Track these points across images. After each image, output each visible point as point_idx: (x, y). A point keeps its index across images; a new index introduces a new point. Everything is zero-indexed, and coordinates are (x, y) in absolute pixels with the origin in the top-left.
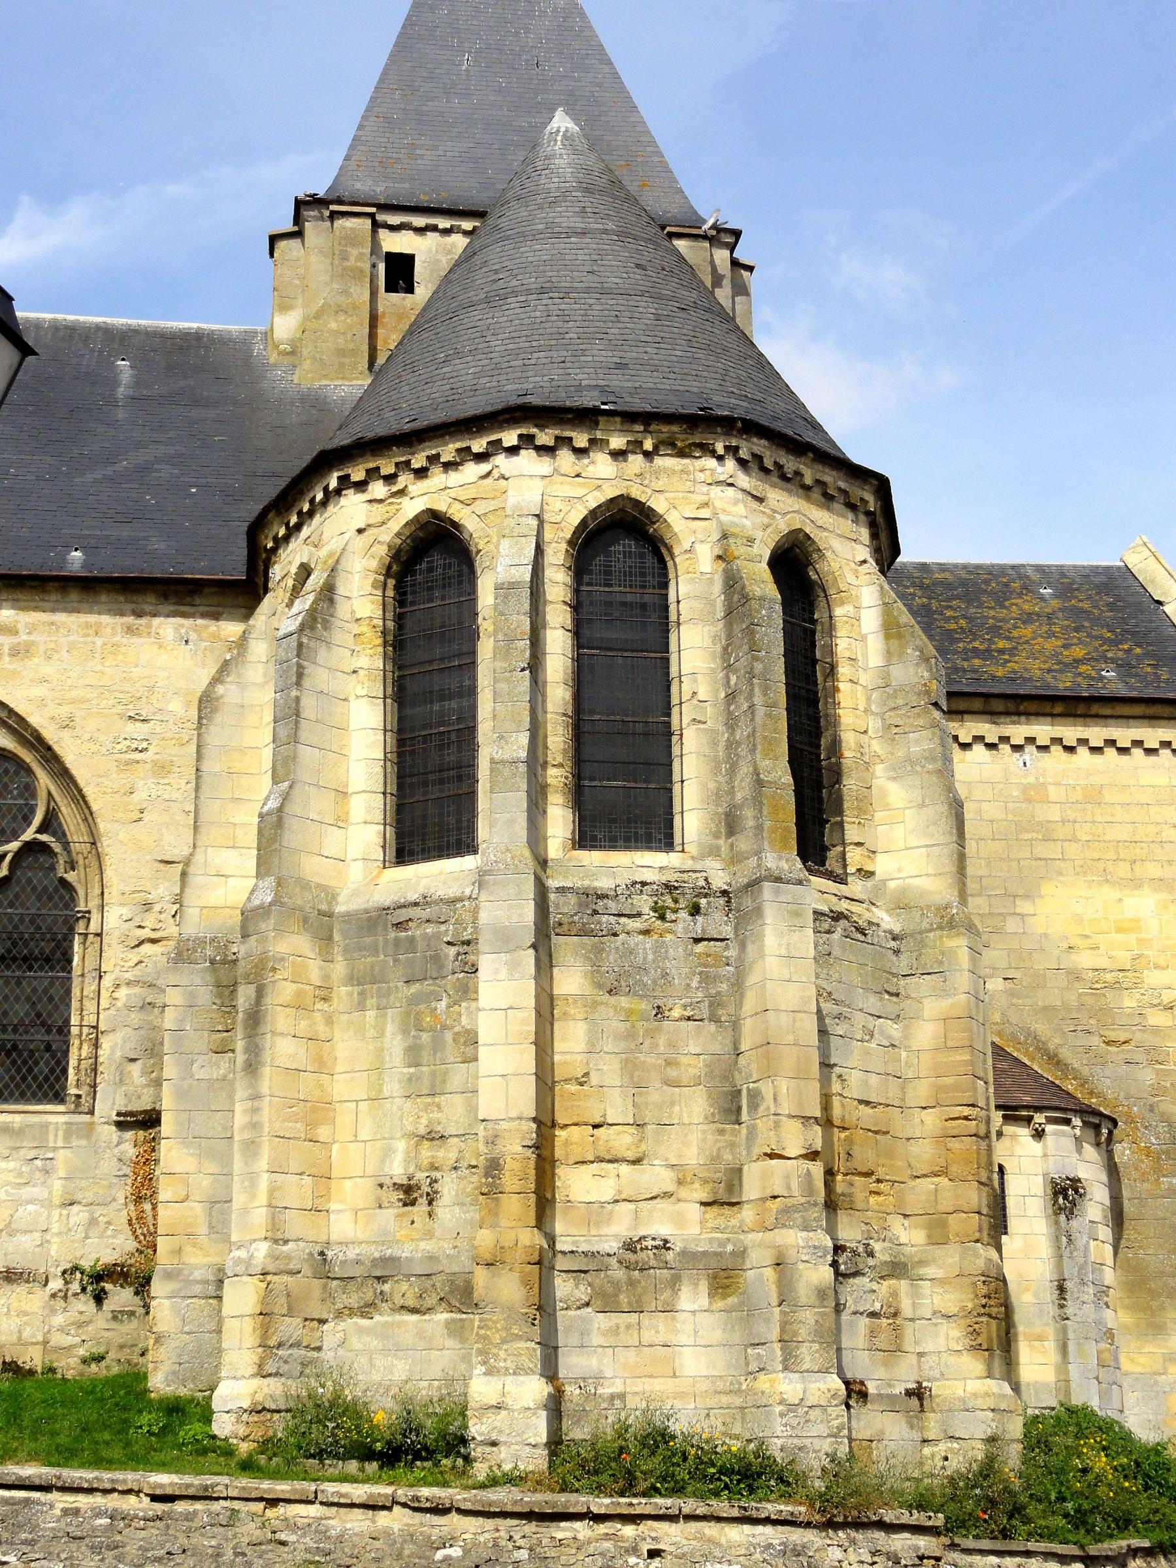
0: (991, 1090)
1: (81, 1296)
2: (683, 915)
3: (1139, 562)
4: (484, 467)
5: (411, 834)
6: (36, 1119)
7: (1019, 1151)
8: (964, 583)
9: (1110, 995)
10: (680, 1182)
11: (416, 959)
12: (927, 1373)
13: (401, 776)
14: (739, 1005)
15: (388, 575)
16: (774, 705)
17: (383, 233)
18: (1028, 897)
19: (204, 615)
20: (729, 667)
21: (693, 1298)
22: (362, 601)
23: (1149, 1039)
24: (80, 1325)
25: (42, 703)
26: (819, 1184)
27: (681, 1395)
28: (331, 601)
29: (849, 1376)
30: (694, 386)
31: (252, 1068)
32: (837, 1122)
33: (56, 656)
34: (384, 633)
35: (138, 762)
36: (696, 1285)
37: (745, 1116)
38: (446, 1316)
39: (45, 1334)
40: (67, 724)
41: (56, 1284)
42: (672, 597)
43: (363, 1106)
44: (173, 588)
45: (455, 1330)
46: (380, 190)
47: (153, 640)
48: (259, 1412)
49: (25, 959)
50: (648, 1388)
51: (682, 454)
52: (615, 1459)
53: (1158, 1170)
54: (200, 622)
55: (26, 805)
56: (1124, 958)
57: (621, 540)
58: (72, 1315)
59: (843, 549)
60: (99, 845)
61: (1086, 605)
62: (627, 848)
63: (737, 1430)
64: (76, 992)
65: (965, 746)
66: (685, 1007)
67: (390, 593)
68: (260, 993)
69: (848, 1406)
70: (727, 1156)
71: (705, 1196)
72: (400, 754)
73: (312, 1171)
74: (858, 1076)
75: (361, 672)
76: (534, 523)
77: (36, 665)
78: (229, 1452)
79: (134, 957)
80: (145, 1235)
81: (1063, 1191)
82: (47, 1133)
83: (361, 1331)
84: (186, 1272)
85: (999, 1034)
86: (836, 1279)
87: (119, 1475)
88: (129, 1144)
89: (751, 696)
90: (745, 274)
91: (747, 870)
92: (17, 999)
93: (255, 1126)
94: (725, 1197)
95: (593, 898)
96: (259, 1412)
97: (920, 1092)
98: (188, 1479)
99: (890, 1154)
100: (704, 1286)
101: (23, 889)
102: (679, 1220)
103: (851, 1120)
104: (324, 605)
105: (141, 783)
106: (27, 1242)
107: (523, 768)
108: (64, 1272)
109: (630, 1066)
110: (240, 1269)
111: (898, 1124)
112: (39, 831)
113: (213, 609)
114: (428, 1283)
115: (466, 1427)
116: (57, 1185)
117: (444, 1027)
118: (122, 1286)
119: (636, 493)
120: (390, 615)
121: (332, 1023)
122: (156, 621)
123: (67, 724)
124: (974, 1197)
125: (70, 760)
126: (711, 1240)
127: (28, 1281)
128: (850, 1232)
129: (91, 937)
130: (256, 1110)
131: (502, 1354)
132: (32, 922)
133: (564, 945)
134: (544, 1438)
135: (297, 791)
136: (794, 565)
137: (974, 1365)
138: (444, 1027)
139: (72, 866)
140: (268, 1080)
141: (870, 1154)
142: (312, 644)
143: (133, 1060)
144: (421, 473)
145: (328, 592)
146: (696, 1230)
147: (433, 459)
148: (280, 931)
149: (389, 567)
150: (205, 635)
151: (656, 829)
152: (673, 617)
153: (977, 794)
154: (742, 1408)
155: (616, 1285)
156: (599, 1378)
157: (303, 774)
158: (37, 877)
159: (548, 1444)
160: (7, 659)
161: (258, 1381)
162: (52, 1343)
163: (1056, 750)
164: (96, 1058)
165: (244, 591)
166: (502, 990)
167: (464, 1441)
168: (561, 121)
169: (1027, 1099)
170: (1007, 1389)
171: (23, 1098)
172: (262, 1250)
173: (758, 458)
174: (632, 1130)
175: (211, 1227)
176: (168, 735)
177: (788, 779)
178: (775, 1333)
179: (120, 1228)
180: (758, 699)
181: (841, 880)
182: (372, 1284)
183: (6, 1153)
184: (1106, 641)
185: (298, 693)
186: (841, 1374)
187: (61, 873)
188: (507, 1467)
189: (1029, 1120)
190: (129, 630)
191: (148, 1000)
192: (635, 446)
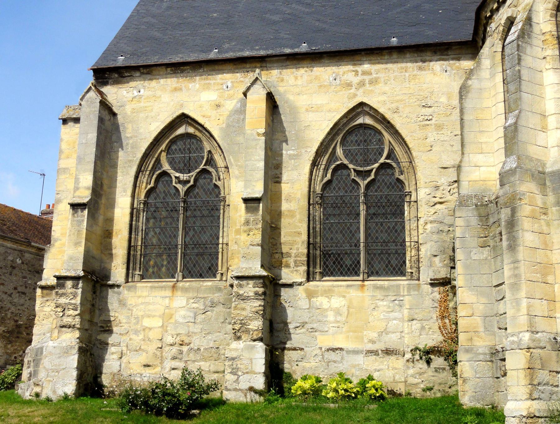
1: (420, 361)
24: (421, 374)
33: (389, 83)
35: (428, 125)
39: (405, 378)
41: (408, 356)
44: (438, 48)
47: (431, 72)
48: (532, 418)
49: (383, 214)
54: (451, 62)
55: (380, 148)
58: (417, 369)
60: (413, 163)
64: (407, 227)
68: (514, 211)
73: (546, 298)
75: (548, 58)
77: (381, 87)
79: (432, 210)
80: (446, 333)
82: (400, 289)
84: (475, 349)
88: (436, 293)
92: (382, 231)
96: (532, 418)
101: (381, 184)
104: (527, 27)
105: (430, 134)
108: (411, 351)
112: (386, 158)
113: (456, 56)
116: (406, 312)
118: (438, 357)
121: (549, 225)
125: (398, 127)
127: (396, 354)
129: (412, 203)
132: (386, 198)
135: (523, 114)
139: (402, 173)
142: (524, 45)
143: (435, 256)
145: (529, 21)
148: (522, 181)
150: (454, 67)
158: (387, 179)
160: (368, 85)
161: (529, 403)
162: (408, 382)
164: (419, 255)
165: (471, 47)
172: (526, 337)
175: (485, 328)
176: (441, 112)
179: (435, 330)
183: (382, 298)
185: (519, 68)
187: (397, 175)
190: (420, 69)
191: (440, 229)
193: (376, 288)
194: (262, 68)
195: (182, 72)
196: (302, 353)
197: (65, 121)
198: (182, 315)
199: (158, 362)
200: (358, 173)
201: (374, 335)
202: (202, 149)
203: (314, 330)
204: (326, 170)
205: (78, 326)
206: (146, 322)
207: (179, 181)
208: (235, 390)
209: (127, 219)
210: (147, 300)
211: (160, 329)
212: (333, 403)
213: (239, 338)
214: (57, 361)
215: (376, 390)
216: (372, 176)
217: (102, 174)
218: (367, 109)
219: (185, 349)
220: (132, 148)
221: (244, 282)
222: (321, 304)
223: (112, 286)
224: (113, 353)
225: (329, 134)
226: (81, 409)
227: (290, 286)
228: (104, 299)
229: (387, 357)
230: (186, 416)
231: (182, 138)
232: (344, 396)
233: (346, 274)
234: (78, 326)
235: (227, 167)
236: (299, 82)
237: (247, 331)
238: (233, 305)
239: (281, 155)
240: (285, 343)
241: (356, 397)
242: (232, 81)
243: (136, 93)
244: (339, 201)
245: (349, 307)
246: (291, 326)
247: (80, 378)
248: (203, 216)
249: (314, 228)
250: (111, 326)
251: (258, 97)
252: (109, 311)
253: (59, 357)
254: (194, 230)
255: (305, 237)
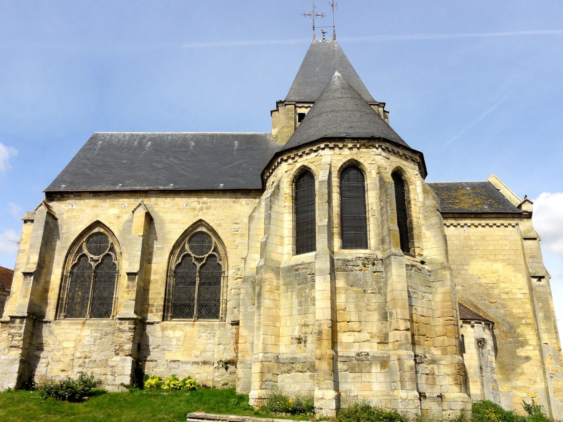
0: (458, 313)
2: (370, 265)
3: (493, 180)
4: (316, 154)
5: (300, 247)
6: (211, 323)
7: (467, 331)
8: (446, 187)
9: (490, 290)
10: (372, 337)
11: (300, 278)
12: (442, 391)
13: (297, 232)
14: (386, 289)
15: (293, 182)
16: (393, 210)
17: (297, 109)
18: (467, 265)
19: (252, 198)
20: (381, 201)
21: (376, 369)
22: (287, 189)
23: (504, 302)
24: (222, 375)
25: (213, 220)
26: (410, 337)
27: (373, 396)
28: (279, 189)
29: (421, 391)
30: (370, 131)
31: (259, 308)
32: (415, 321)
34: (292, 197)
36: (377, 366)
37: (389, 319)
38: (309, 373)
40: (219, 225)
41: (216, 365)
42: (366, 184)
43: (288, 317)
45: (312, 377)
46: (297, 99)
50: (364, 394)
51: (367, 148)
52: (354, 414)
53: (506, 337)
56: (494, 280)
57: (352, 171)
58: (220, 373)
59: (411, 171)
61: (479, 191)
62: (356, 249)
63: (389, 406)
64: (222, 291)
65: (448, 226)
66: (371, 290)
67: (294, 187)
69: (420, 400)
70: (384, 330)
71: (378, 341)
72: (297, 227)
74: (420, 308)
76: (329, 166)
77: (212, 211)
78: (252, 410)
79: (235, 282)
81: (480, 342)
83: (288, 377)
85: (461, 301)
86: (415, 364)
87: (221, 416)
89: (387, 207)
90: (387, 114)
91: (388, 253)
93: (259, 323)
94: (384, 341)
95: (346, 262)
97: (438, 313)
98: (239, 417)
99: (430, 330)
100: (379, 366)
102: (371, 347)
103: (419, 320)
106: (209, 354)
107: (326, 227)
109: (357, 306)
110: (256, 361)
111: (432, 322)
112: (213, 251)
114: (305, 364)
115: (313, 404)
116: (216, 340)
117: (308, 296)
119: (355, 158)
120: (294, 192)
122: (241, 200)
123: (219, 225)
124: (454, 342)
125: (220, 234)
126: (380, 353)
128: (419, 351)
130: (259, 319)
131: (323, 384)
133: (339, 274)
134: (334, 407)
135: (270, 236)
136: (398, 176)
137: (456, 389)
138: (308, 296)
140: (263, 310)
141: (424, 330)
144: (301, 156)
145: (278, 187)
146: (376, 350)
147: (304, 153)
149: (293, 180)
151: (364, 244)
152: (366, 189)
153: (452, 239)
154: (390, 400)
155: (354, 365)
156: (350, 391)
157: (271, 232)
158: (212, 263)
159: (336, 409)
161: (260, 391)
163: (473, 227)
165: (260, 191)
166: (322, 285)
167: (313, 408)
168: (337, 74)
169: (469, 317)
170: (466, 396)
171: (209, 318)
173: (387, 148)
174: (358, 323)
177: (398, 229)
178: (399, 379)
180: (389, 208)
181: (414, 257)
182: (290, 365)
184: (485, 199)
186: (418, 390)
188: (325, 415)
189: (470, 323)
190: (234, 202)
192: (355, 146)
193: (201, 325)
194: (146, 197)
195: (99, 196)
196: (156, 363)
197: (25, 221)
198: (87, 340)
199: (70, 369)
200: (197, 259)
201: (197, 353)
202: (108, 241)
203: (164, 350)
204: (179, 257)
205: (21, 346)
206: (65, 344)
207: (92, 260)
208: (113, 385)
209: (59, 281)
210: (67, 331)
211: (73, 349)
212: (166, 392)
213: (118, 354)
214: (5, 368)
215: (191, 384)
216: (204, 262)
217: (45, 254)
218: (204, 223)
219: (87, 360)
220: (65, 239)
221: (123, 322)
222: (169, 334)
223: (46, 322)
224: (43, 363)
225: (181, 236)
226: (17, 397)
227: (152, 324)
228: (40, 330)
229: (204, 366)
230: (80, 400)
231: (96, 236)
232: (173, 388)
233: (186, 317)
234: (21, 346)
235: (121, 253)
236: (166, 206)
237: (123, 350)
238: (116, 335)
239: (153, 247)
240: (147, 357)
241: (180, 389)
242: (129, 203)
243: (70, 207)
244: (185, 275)
245: (185, 336)
246: (151, 347)
247: (19, 378)
248: (105, 281)
249: (169, 290)
250: (43, 346)
251: (140, 214)
252: (42, 337)
253: (7, 366)
254: (99, 289)
255: (163, 295)
